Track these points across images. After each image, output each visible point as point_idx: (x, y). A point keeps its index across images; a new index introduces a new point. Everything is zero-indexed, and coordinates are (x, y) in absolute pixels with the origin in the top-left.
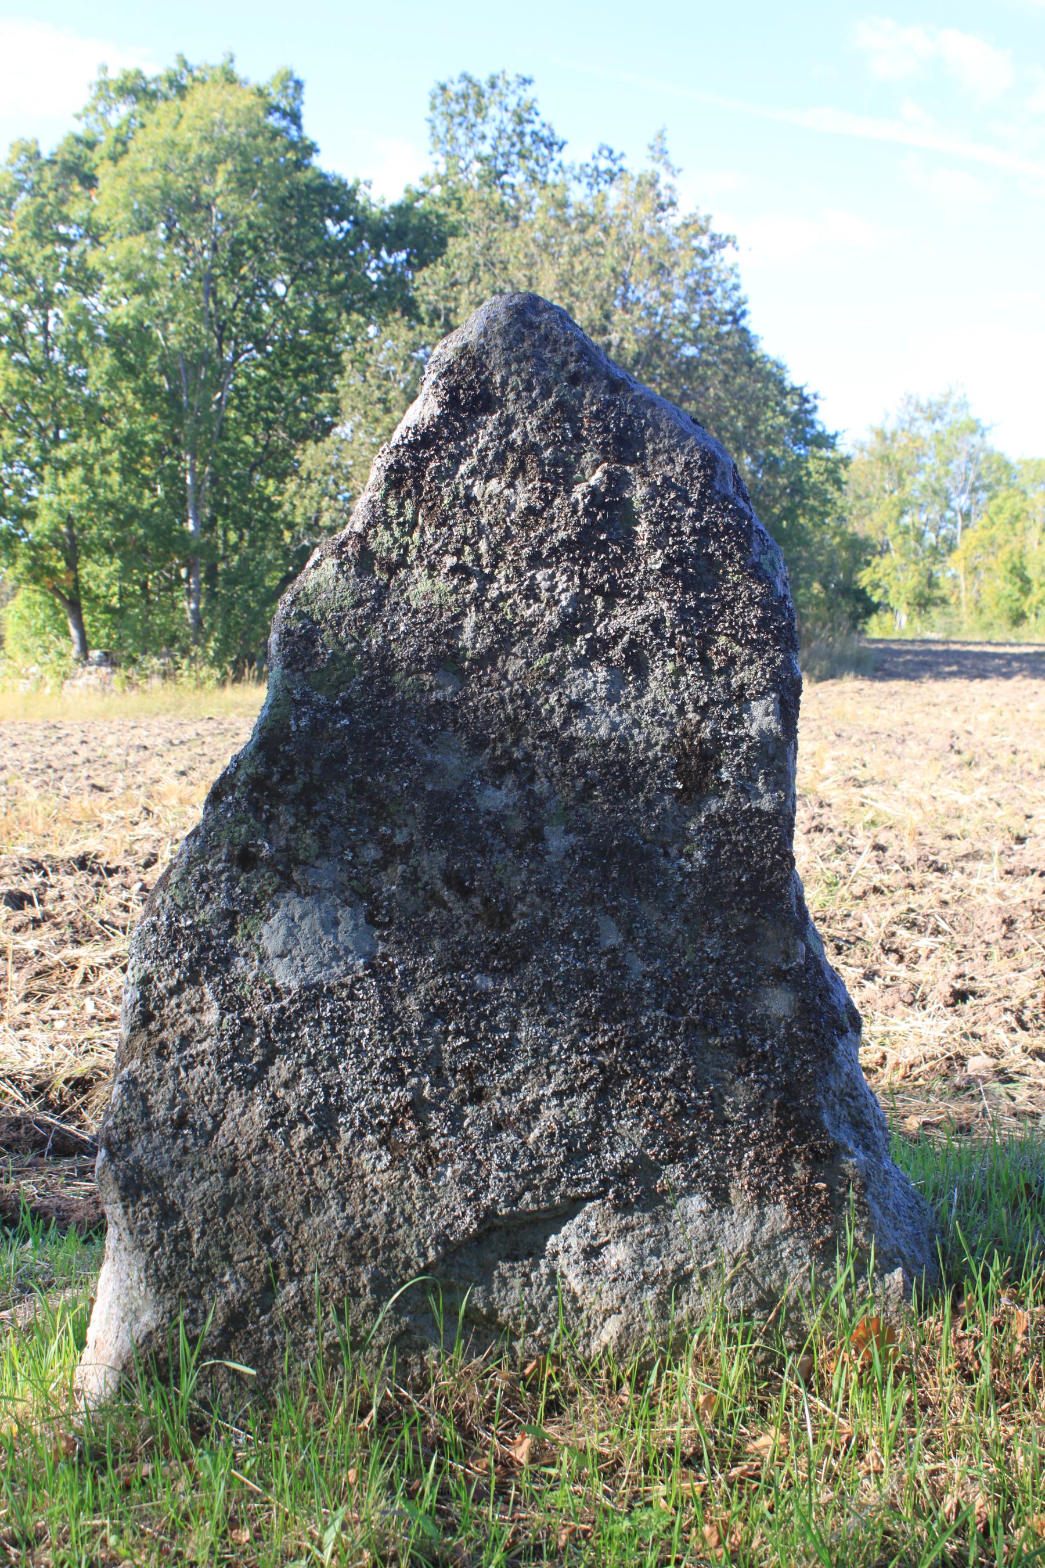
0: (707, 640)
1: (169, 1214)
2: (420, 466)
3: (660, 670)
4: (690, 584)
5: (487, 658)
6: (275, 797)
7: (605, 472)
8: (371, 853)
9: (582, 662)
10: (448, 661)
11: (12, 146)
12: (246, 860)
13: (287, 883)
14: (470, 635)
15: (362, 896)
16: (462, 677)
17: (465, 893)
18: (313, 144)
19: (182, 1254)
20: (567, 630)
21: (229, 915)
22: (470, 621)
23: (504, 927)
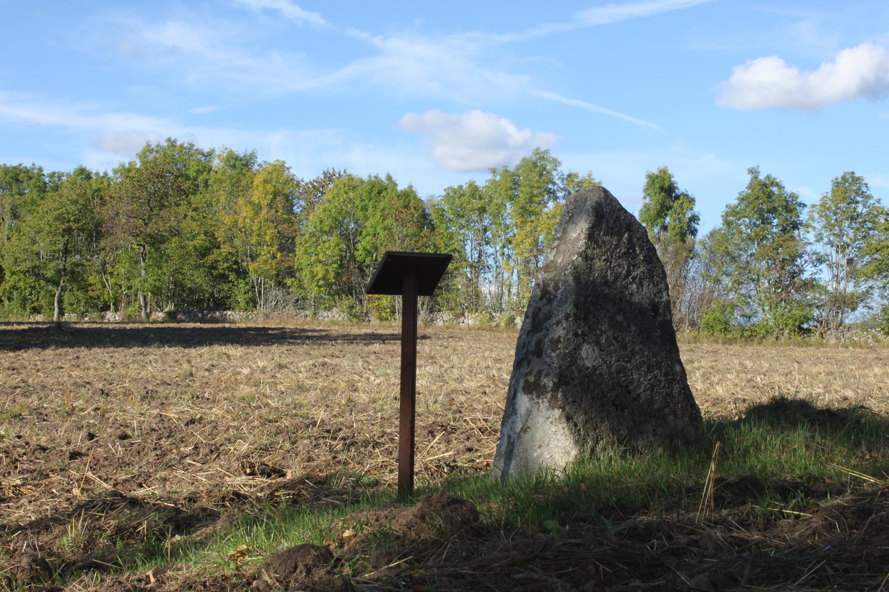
0: (653, 277)
1: (576, 425)
2: (594, 232)
3: (646, 284)
4: (648, 264)
5: (614, 282)
6: (580, 319)
7: (78, 290)
8: (598, 332)
9: (631, 283)
10: (606, 283)
11: (664, 171)
12: (576, 335)
13: (584, 341)
14: (610, 278)
15: (597, 343)
16: (609, 287)
17: (618, 342)
18: (837, 184)
19: (580, 435)
20: (627, 276)
21: (575, 349)
22: (609, 273)
23: (626, 350)
